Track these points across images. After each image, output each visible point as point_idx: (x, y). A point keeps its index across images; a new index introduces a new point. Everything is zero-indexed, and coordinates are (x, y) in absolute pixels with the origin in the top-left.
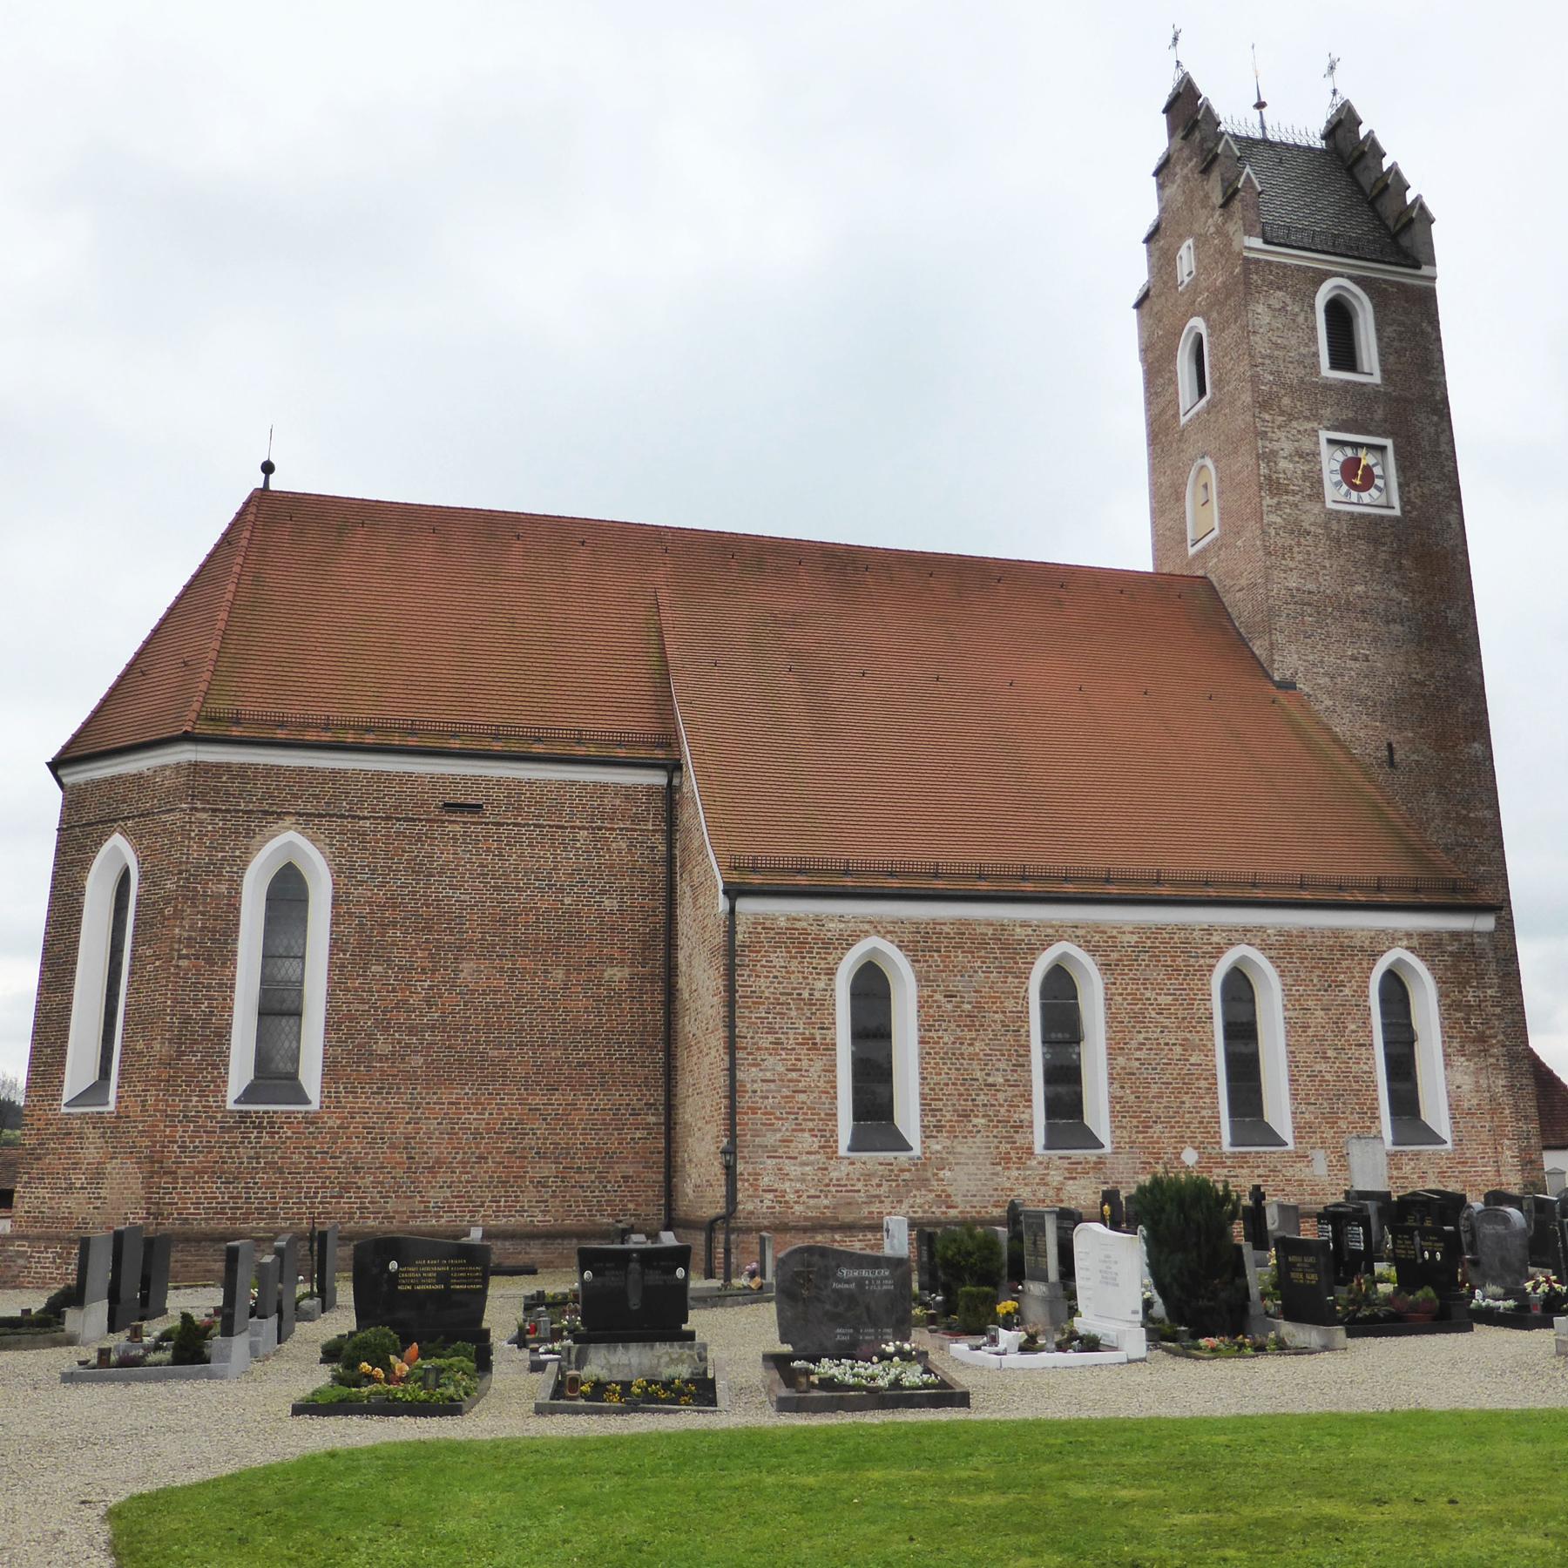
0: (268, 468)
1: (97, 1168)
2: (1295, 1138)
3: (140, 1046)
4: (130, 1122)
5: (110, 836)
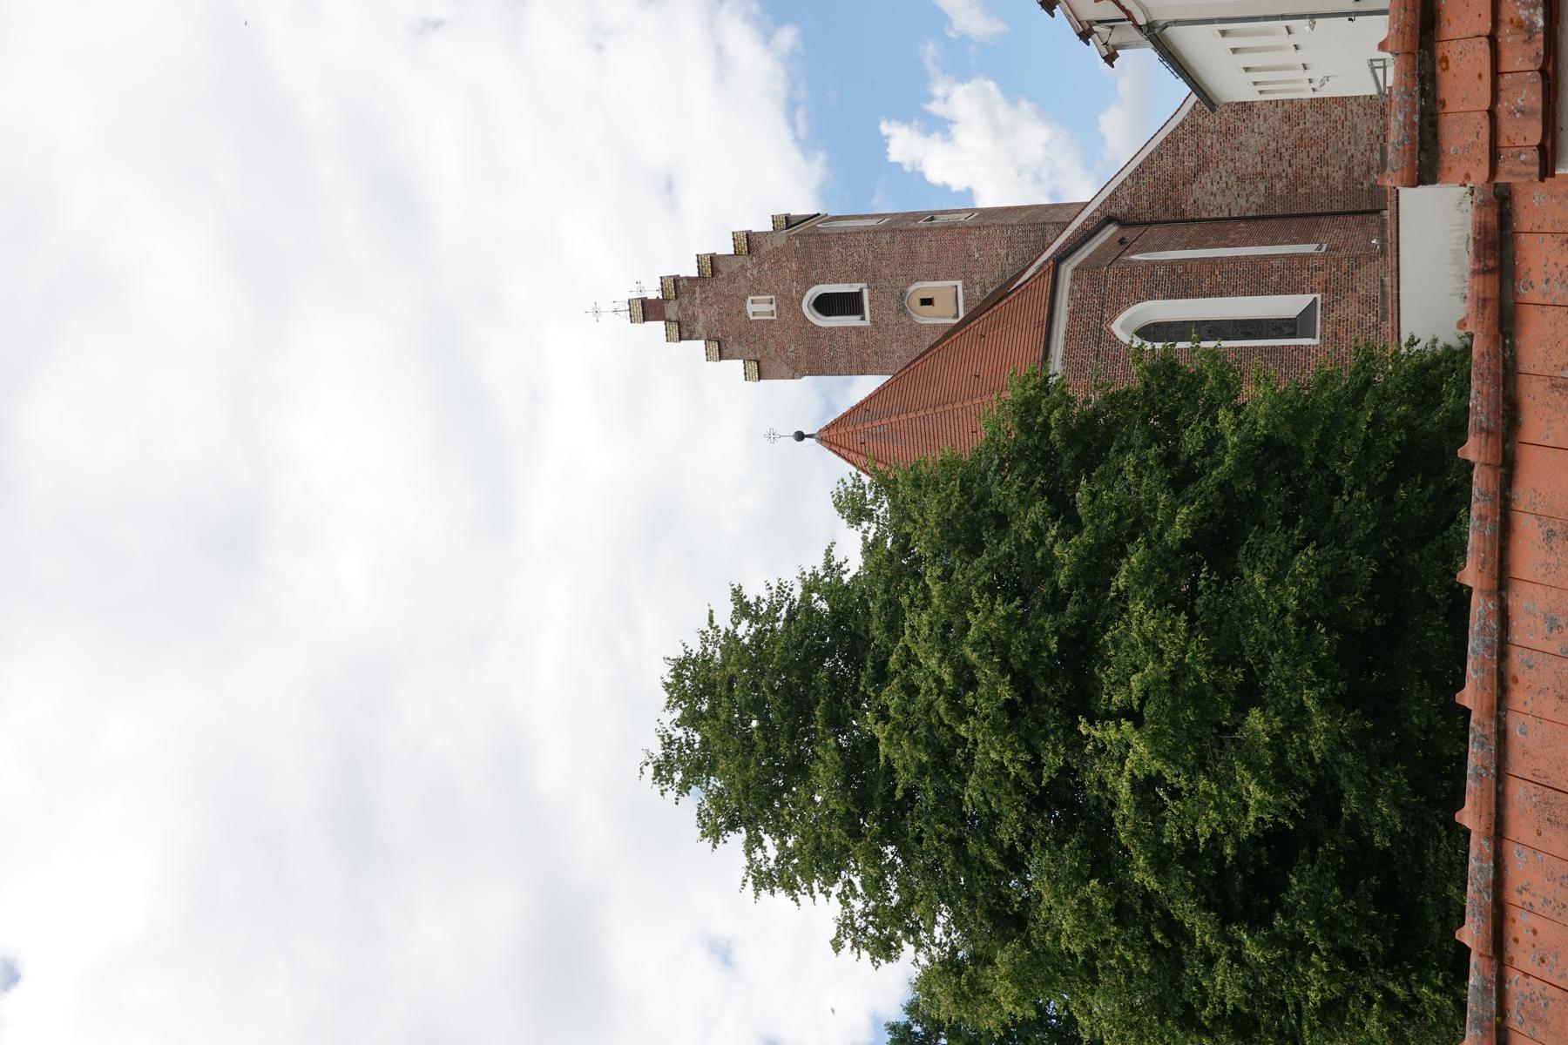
0: (800, 436)
1: (1363, 304)
2: (1311, 292)
3: (1275, 278)
4: (1330, 279)
5: (1112, 333)
